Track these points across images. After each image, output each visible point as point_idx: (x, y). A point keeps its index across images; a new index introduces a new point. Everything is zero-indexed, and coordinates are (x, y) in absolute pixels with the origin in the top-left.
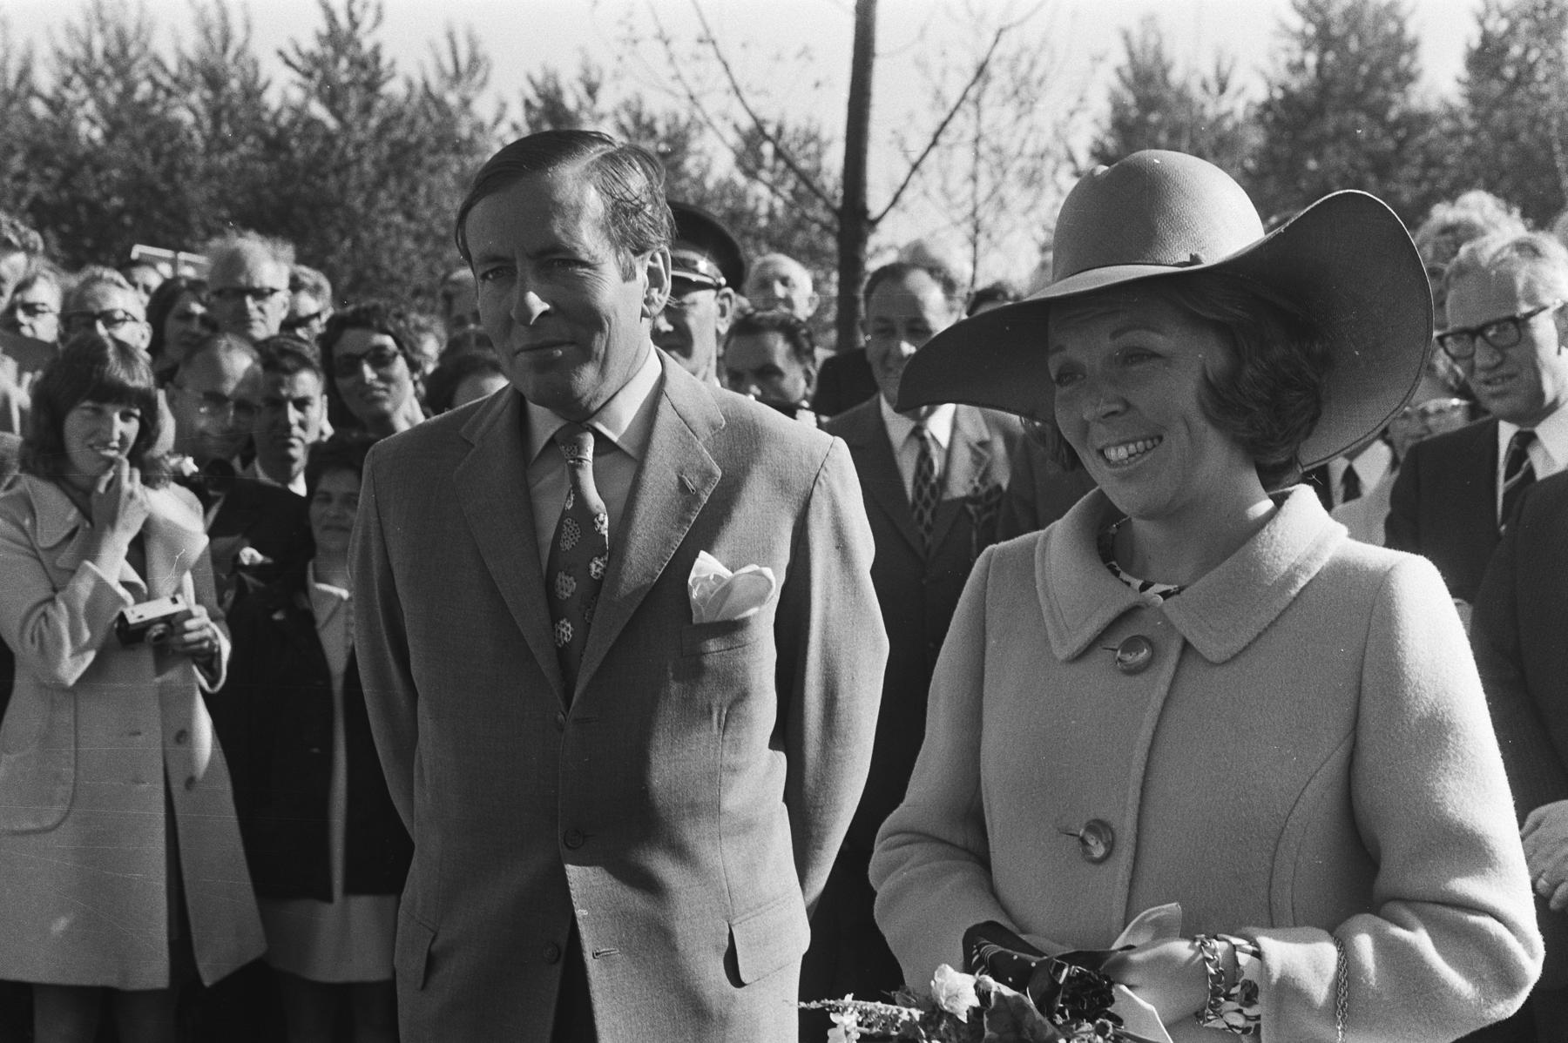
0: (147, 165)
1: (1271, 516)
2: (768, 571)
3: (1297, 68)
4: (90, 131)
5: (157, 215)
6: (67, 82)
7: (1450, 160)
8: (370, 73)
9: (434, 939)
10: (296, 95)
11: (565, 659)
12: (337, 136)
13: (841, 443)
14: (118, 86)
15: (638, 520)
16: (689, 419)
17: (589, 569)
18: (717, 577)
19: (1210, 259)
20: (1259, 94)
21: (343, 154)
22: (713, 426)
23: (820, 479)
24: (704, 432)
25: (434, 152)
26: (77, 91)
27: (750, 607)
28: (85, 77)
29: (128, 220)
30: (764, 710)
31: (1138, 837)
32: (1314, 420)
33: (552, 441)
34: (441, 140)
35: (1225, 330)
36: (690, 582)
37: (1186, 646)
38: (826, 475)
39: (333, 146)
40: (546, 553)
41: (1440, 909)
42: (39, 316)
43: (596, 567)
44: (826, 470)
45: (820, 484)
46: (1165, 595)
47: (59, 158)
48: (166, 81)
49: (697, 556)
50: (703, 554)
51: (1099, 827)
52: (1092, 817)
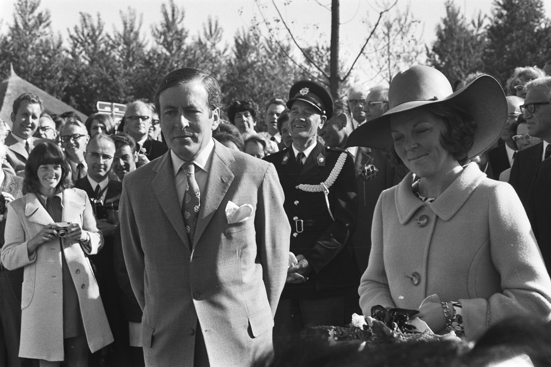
0: (104, 71)
1: (462, 172)
2: (250, 206)
3: (500, 16)
4: (84, 60)
5: (109, 89)
6: (75, 46)
8: (180, 36)
9: (154, 331)
11: (189, 237)
12: (169, 59)
13: (272, 164)
14: (93, 46)
15: (209, 193)
16: (223, 160)
17: (194, 209)
18: (234, 209)
21: (171, 65)
22: (231, 161)
23: (266, 176)
24: (228, 163)
25: (203, 62)
26: (79, 48)
27: (245, 217)
28: (81, 43)
29: (98, 91)
30: (253, 250)
32: (472, 145)
33: (181, 169)
34: (205, 58)
35: (445, 119)
36: (226, 210)
37: (437, 217)
38: (268, 175)
39: (168, 62)
40: (181, 205)
41: (520, 291)
42: (47, 130)
43: (196, 208)
44: (267, 173)
45: (266, 178)
46: (431, 201)
47: (74, 72)
48: (111, 43)
49: (228, 203)
50: (229, 202)
51: (416, 274)
52: (414, 271)
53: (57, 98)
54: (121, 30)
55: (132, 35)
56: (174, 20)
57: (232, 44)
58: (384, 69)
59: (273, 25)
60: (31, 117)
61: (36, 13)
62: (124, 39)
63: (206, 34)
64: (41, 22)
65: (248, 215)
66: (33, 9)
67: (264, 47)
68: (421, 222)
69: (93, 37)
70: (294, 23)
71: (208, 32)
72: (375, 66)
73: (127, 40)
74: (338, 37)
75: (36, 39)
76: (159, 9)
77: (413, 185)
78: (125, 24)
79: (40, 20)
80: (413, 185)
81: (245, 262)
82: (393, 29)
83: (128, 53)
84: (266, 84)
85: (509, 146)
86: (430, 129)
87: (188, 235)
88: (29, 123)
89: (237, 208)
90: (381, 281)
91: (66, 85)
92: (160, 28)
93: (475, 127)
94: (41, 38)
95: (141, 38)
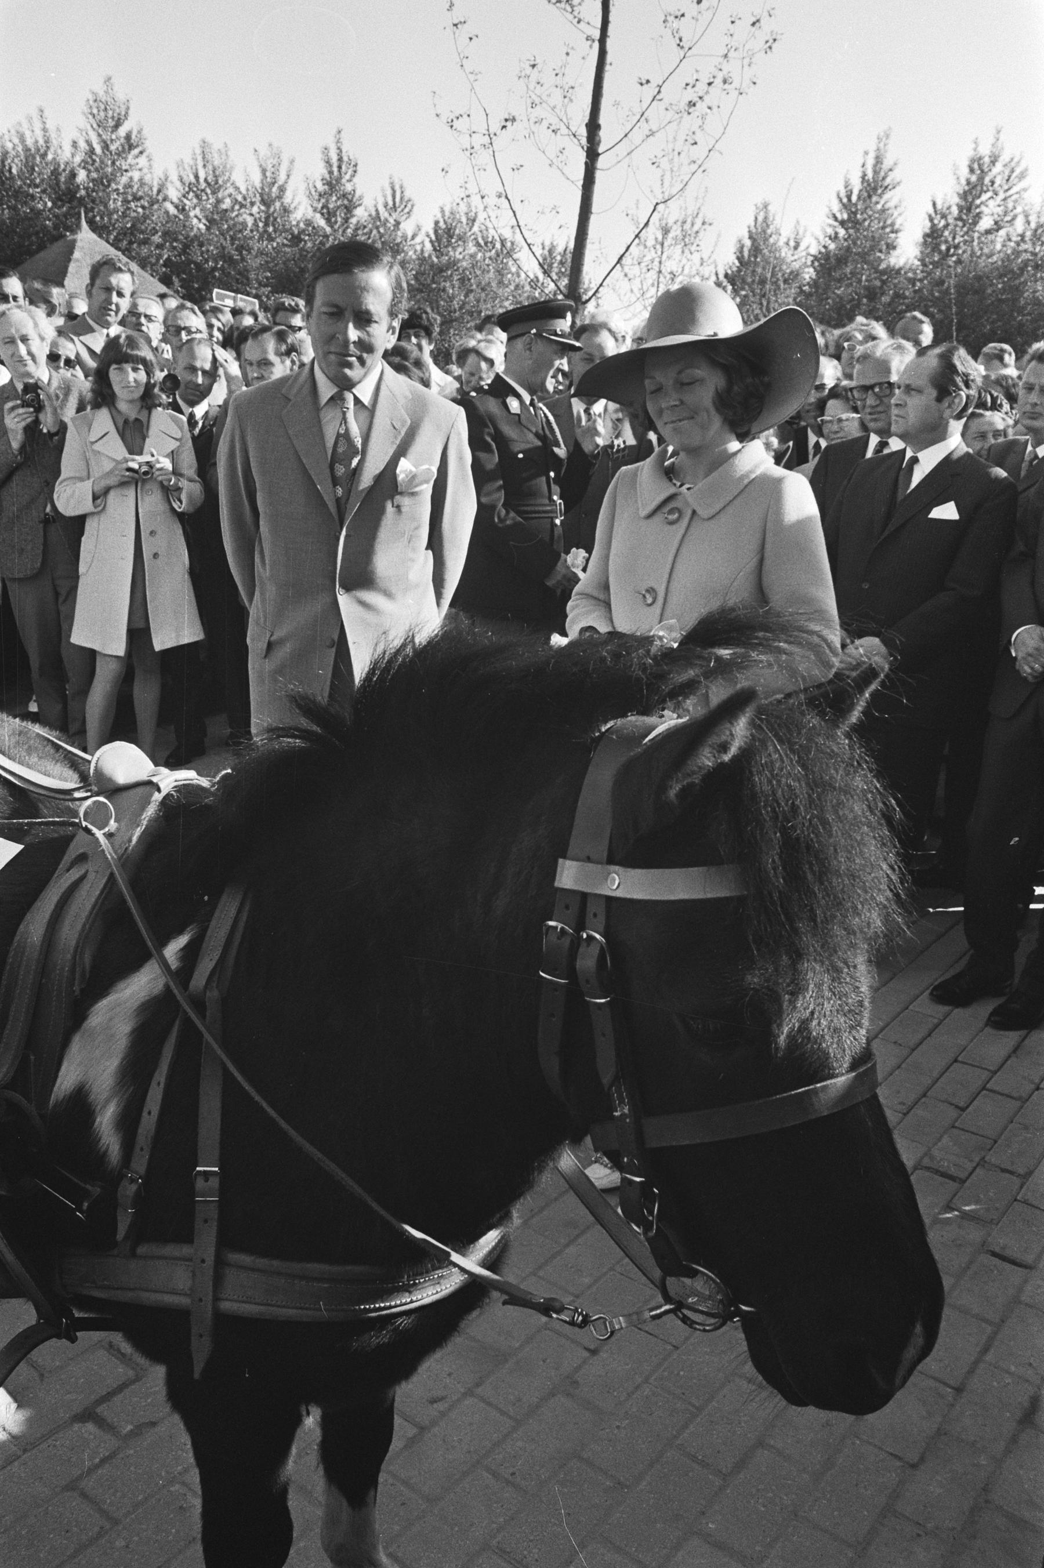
0: (227, 244)
3: (835, 238)
4: (199, 225)
7: (907, 293)
10: (310, 214)
18: (411, 472)
19: (722, 335)
20: (814, 251)
22: (406, 397)
24: (402, 401)
31: (666, 594)
32: (759, 413)
33: (332, 398)
35: (726, 369)
36: (398, 471)
37: (694, 512)
43: (355, 462)
46: (688, 489)
47: (181, 237)
48: (240, 198)
50: (402, 459)
51: (651, 591)
53: (152, 276)
54: (256, 178)
55: (275, 189)
56: (340, 178)
57: (429, 228)
58: (648, 295)
59: (492, 200)
60: (114, 294)
61: (122, 131)
62: (261, 195)
63: (386, 205)
64: (131, 147)
65: (427, 482)
66: (117, 125)
67: (475, 239)
68: (670, 517)
69: (215, 187)
70: (526, 203)
71: (391, 203)
72: (636, 290)
73: (266, 197)
74: (587, 234)
75: (122, 175)
76: (319, 156)
77: (666, 463)
78: (264, 171)
79: (129, 144)
80: (666, 463)
81: (414, 550)
82: (671, 235)
83: (267, 218)
84: (471, 296)
85: (813, 432)
86: (702, 381)
87: (338, 500)
88: (111, 304)
89: (414, 469)
90: (602, 597)
91: (166, 256)
92: (321, 187)
93: (768, 386)
94: (129, 174)
95: (288, 198)
